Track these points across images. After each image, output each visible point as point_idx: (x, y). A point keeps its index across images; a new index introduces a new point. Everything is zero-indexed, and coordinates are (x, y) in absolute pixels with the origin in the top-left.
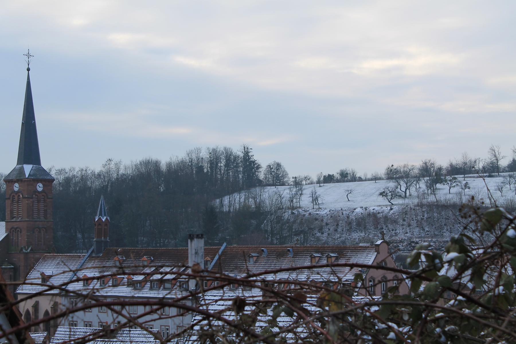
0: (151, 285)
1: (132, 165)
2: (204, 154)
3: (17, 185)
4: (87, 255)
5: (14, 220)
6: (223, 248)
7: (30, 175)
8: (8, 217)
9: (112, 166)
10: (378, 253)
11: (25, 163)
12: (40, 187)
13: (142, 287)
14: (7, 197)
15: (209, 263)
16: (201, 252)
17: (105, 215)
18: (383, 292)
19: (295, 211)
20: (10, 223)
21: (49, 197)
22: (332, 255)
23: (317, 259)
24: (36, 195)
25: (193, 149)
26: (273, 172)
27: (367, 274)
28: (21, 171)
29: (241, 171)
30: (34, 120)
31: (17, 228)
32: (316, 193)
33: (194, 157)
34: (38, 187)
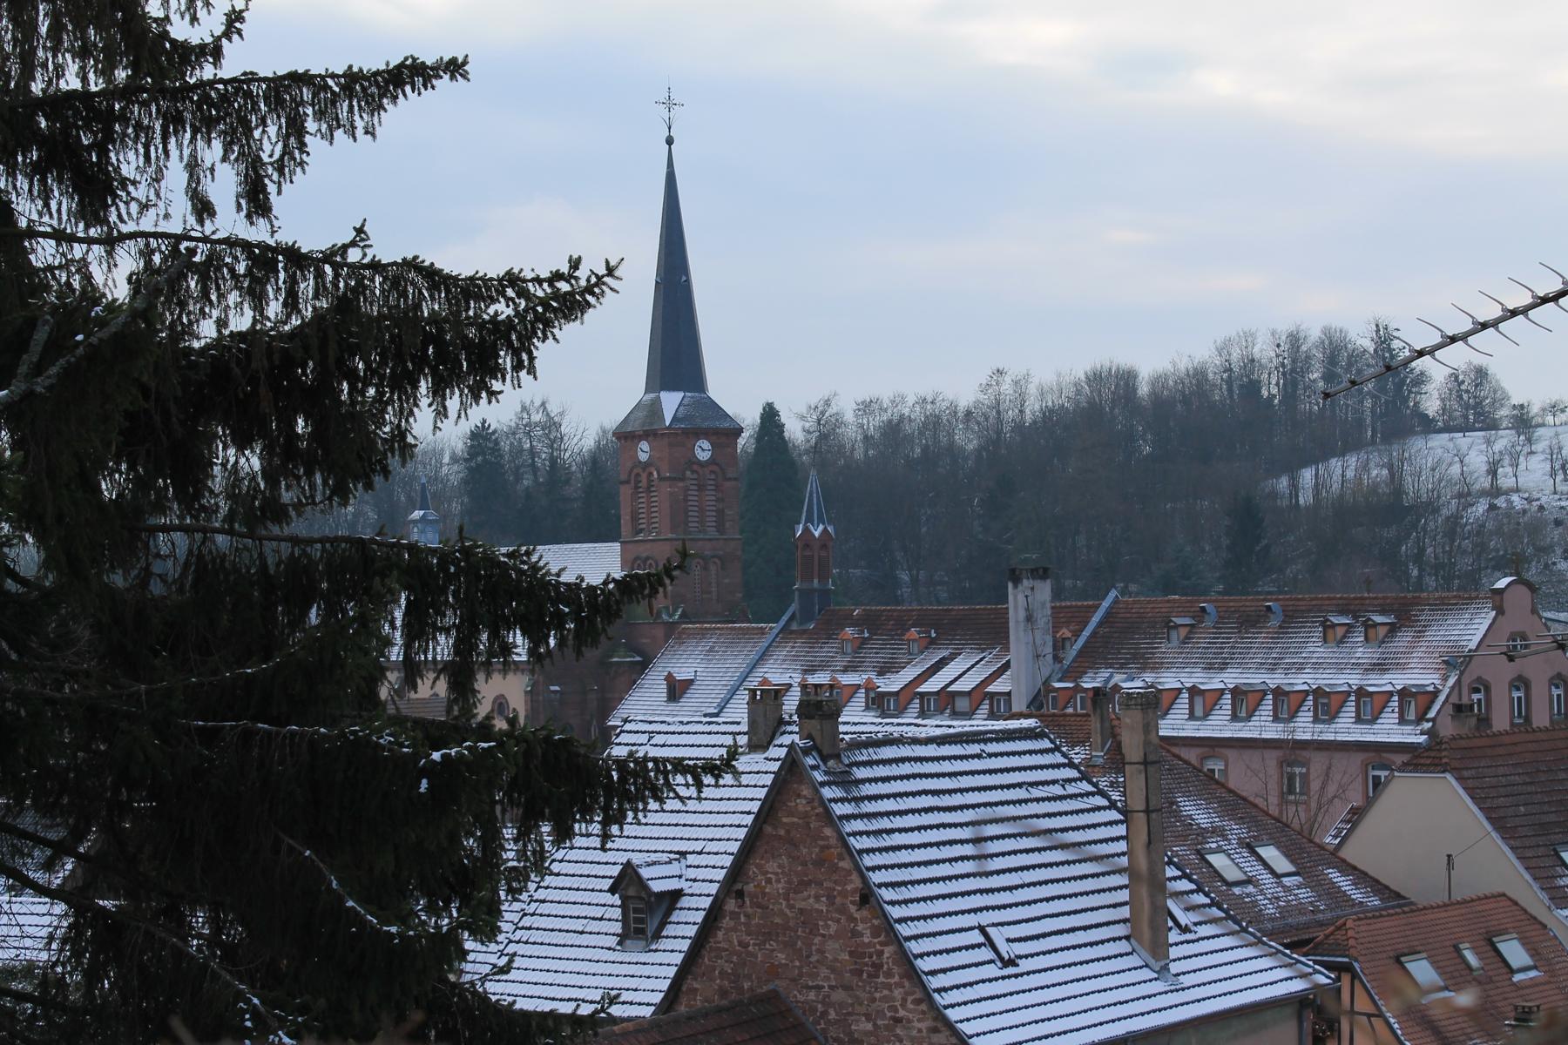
0: (991, 705)
1: (1059, 384)
2: (1264, 350)
3: (644, 445)
4: (776, 627)
6: (1106, 604)
7: (675, 419)
8: (626, 529)
9: (1007, 387)
10: (1500, 611)
11: (663, 389)
12: (703, 450)
13: (901, 711)
14: (623, 477)
15: (1068, 644)
16: (1044, 617)
17: (821, 521)
18: (1517, 721)
19: (1501, 502)
20: (630, 546)
21: (730, 475)
22: (1379, 619)
23: (1340, 631)
24: (693, 472)
25: (1234, 334)
26: (1467, 391)
27: (1462, 673)
28: (655, 409)
29: (1366, 390)
31: (648, 558)
32: (1560, 448)
33: (1236, 355)
34: (698, 451)
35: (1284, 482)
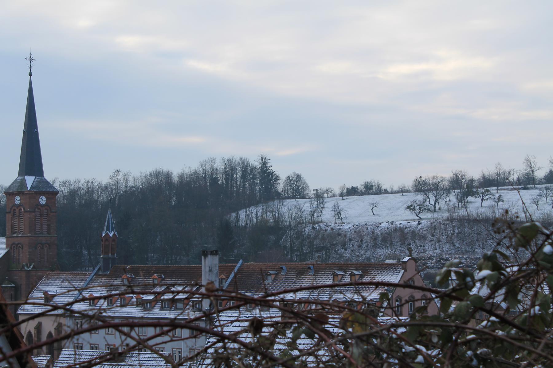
0: (162, 305)
1: (141, 177)
2: (219, 165)
3: (18, 198)
4: (93, 273)
5: (15, 235)
6: (238, 265)
7: (32, 187)
8: (8, 232)
9: (120, 177)
10: (405, 270)
12: (43, 200)
13: (153, 308)
14: (8, 210)
15: (224, 281)
16: (216, 270)
17: (112, 230)
18: (410, 313)
19: (316, 226)
20: (10, 239)
21: (53, 211)
22: (356, 273)
23: (340, 277)
26: (293, 184)
27: (393, 294)
28: (23, 183)
29: (259, 183)
30: (37, 128)
31: (18, 244)
32: (338, 206)
33: (208, 168)
34: (40, 200)
35: (233, 215)
